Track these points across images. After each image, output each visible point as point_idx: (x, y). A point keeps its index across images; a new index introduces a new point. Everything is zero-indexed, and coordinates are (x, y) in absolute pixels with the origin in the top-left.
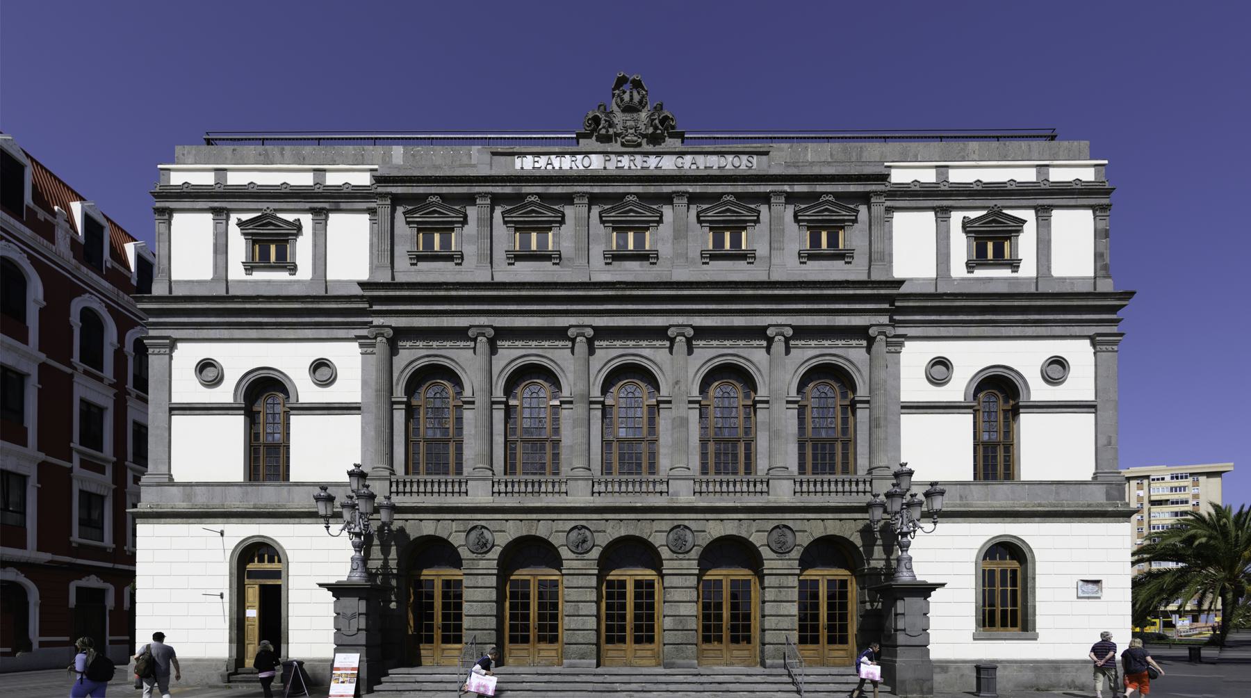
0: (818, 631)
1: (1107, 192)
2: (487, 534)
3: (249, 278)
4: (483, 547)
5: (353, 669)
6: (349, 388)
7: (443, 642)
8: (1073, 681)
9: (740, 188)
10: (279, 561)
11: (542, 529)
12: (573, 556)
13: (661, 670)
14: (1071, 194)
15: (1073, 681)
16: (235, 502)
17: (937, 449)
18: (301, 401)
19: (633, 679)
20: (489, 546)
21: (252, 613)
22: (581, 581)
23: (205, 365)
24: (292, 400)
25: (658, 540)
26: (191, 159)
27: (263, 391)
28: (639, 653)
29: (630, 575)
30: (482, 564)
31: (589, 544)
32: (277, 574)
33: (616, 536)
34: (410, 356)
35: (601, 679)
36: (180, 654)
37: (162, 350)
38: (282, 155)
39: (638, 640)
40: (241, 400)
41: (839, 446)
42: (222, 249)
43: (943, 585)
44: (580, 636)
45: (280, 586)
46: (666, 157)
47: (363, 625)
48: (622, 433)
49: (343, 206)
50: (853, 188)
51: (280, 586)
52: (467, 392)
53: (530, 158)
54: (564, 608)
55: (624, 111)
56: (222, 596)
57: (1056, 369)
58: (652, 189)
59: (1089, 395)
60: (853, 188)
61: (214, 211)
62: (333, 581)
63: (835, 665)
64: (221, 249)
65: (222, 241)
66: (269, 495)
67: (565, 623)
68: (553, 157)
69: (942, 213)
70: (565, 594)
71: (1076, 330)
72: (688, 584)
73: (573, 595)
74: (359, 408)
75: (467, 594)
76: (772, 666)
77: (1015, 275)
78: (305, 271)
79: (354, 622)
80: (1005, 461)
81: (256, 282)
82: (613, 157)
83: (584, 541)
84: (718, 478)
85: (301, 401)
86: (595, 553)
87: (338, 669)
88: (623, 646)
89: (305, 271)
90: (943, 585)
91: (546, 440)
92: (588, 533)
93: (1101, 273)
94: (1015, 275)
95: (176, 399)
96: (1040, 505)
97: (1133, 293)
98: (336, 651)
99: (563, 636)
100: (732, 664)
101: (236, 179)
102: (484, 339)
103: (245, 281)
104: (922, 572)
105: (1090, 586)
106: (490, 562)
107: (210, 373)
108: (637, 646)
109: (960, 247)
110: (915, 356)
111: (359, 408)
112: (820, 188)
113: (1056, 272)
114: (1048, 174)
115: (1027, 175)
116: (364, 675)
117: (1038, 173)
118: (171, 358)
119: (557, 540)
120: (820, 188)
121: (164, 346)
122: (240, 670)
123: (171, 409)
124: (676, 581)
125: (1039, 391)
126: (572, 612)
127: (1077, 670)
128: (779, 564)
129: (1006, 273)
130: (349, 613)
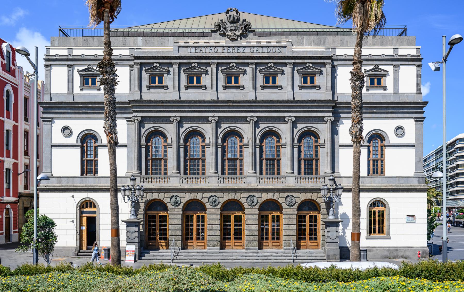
0: (306, 235)
1: (421, 60)
2: (178, 199)
3: (81, 92)
4: (177, 204)
5: (133, 251)
6: (410, 137)
8: (403, 255)
9: (275, 61)
10: (95, 207)
12: (211, 207)
13: (244, 251)
15: (403, 255)
16: (78, 184)
18: (103, 143)
19: (234, 254)
20: (179, 203)
21: (84, 228)
22: (213, 216)
23: (65, 129)
24: (99, 142)
25: (243, 200)
26: (81, 45)
27: (87, 136)
28: (236, 244)
30: (176, 210)
31: (217, 202)
32: (95, 212)
33: (227, 199)
35: (222, 254)
37: (48, 123)
38: (93, 40)
41: (314, 162)
42: (71, 80)
44: (213, 238)
45: (95, 218)
46: (246, 48)
47: (137, 235)
48: (230, 156)
49: (119, 63)
50: (319, 61)
51: (95, 218)
52: (169, 141)
53: (194, 48)
54: (207, 227)
55: (230, 23)
56: (73, 221)
58: (241, 61)
59: (413, 141)
60: (319, 61)
61: (68, 66)
62: (125, 220)
63: (312, 249)
64: (71, 81)
65: (71, 77)
66: (90, 181)
67: (207, 233)
68: (203, 48)
70: (207, 221)
72: (254, 218)
73: (211, 222)
74: (126, 146)
75: (170, 222)
78: (390, 89)
79: (134, 234)
80: (381, 166)
82: (226, 48)
83: (215, 201)
84: (266, 176)
85: (103, 143)
86: (219, 206)
87: (128, 251)
88: (230, 241)
89: (390, 89)
91: (199, 159)
92: (216, 198)
95: (53, 142)
96: (392, 186)
97: (427, 102)
98: (127, 244)
99: (207, 238)
100: (273, 248)
101: (77, 52)
102: (176, 121)
105: (411, 218)
106: (179, 210)
107: (67, 132)
108: (236, 241)
110: (59, 124)
111: (126, 146)
112: (306, 61)
113: (401, 91)
114: (398, 51)
115: (389, 52)
116: (137, 253)
118: (51, 126)
119: (205, 200)
120: (306, 61)
121: (49, 121)
122: (81, 251)
123: (52, 146)
124: (250, 217)
125: (392, 139)
126: (210, 228)
127: (405, 251)
128: (289, 210)
129: (382, 91)
130: (132, 231)
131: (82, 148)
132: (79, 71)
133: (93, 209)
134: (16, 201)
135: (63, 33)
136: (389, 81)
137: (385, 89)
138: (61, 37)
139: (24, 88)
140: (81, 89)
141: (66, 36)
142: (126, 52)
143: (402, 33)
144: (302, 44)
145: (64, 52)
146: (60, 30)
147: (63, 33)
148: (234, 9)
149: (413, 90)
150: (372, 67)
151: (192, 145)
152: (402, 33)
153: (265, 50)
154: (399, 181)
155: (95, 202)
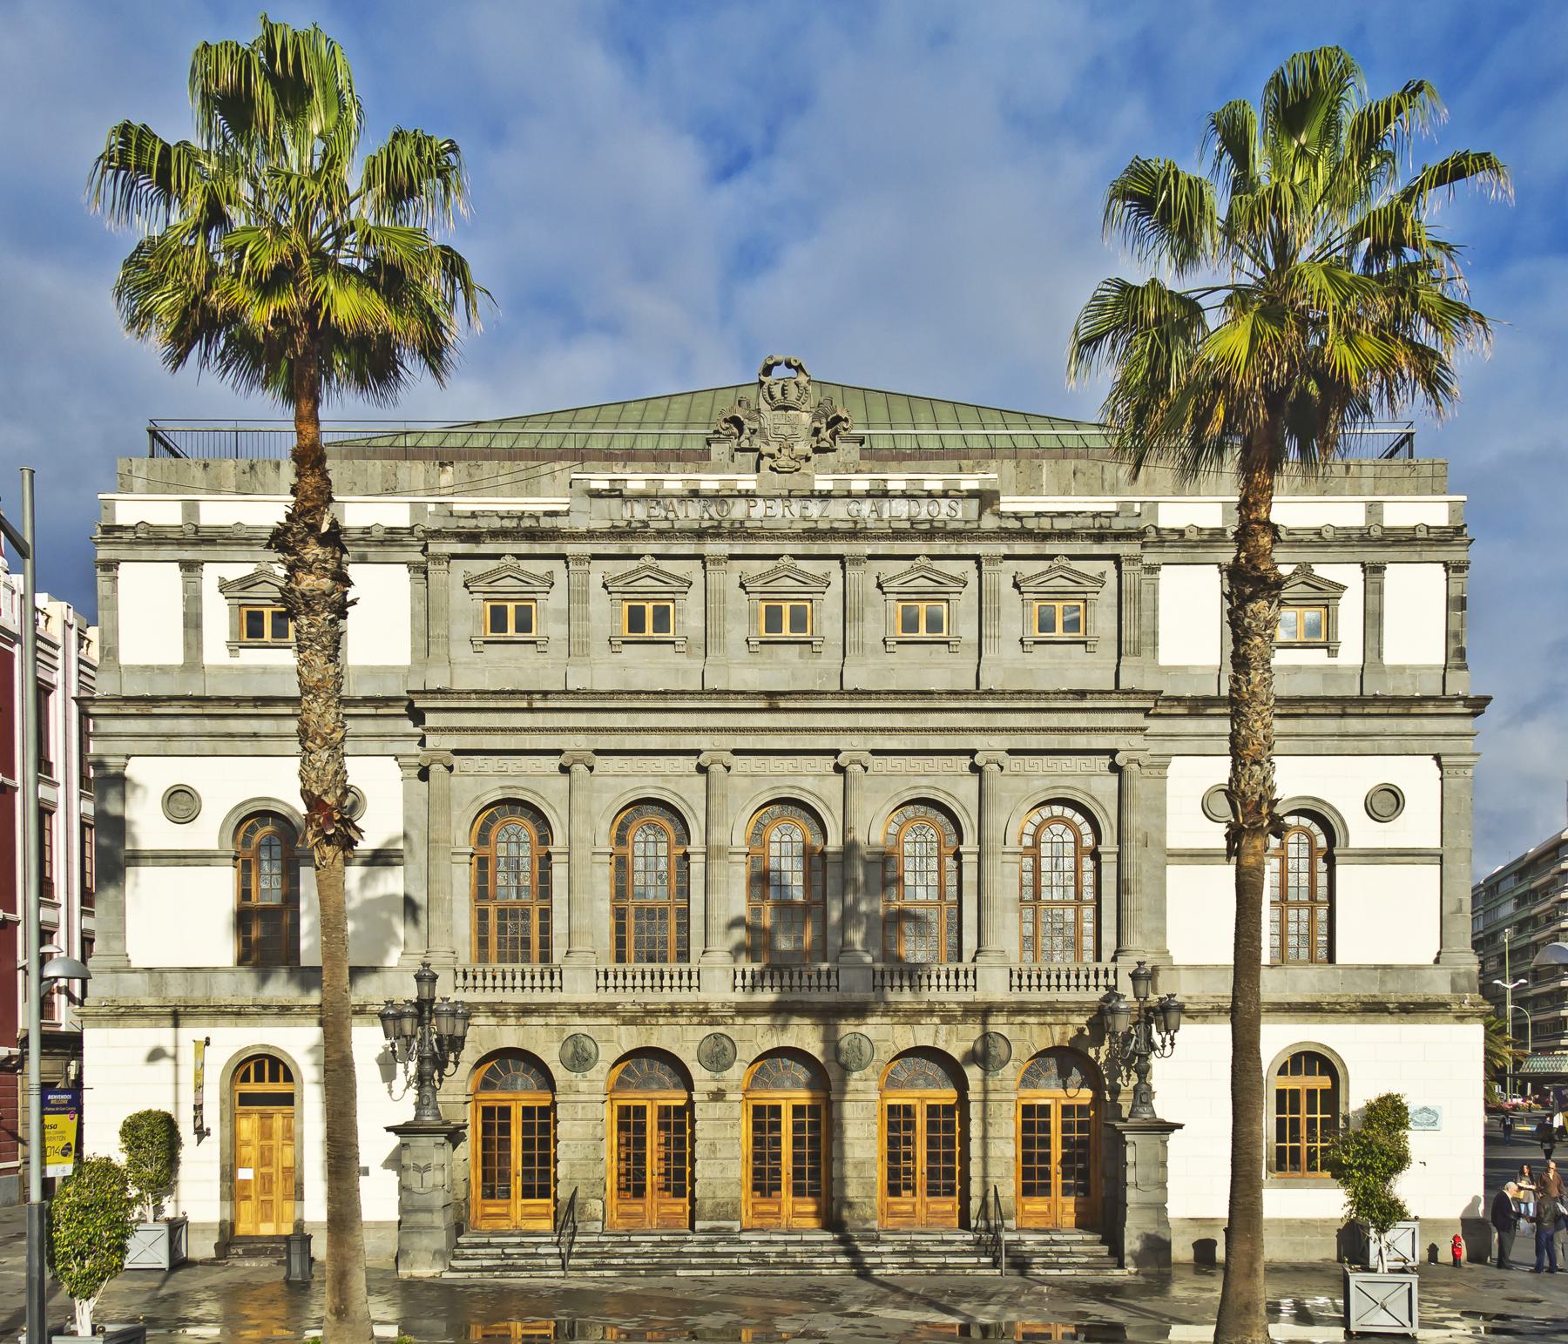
6: (1419, 824)
7: (525, 1196)
10: (289, 1077)
11: (663, 1037)
14: (1408, 541)
17: (1195, 922)
29: (520, 1097)
34: (483, 782)
36: (192, 1219)
39: (528, 1192)
40: (230, 848)
43: (1180, 1126)
57: (1386, 802)
64: (193, 623)
69: (189, 567)
71: (1415, 745)
76: (703, 1231)
77: (1332, 661)
81: (246, 670)
89: (1351, 653)
90: (1180, 1126)
93: (1454, 662)
94: (1332, 661)
97: (1488, 699)
103: (230, 668)
104: (1163, 1109)
109: (218, 617)
112: (1049, 548)
117: (185, 508)
120: (1049, 548)
125: (1362, 832)
131: (245, 868)
132: (224, 586)
133: (280, 1087)
134: (10, 1058)
135: (166, 446)
136: (1350, 611)
137: (1331, 648)
138: (156, 461)
139: (59, 654)
140: (235, 647)
141: (177, 456)
142: (393, 513)
143: (1397, 448)
144: (1032, 488)
145: (165, 512)
146: (153, 433)
147: (166, 446)
148: (778, 358)
149: (1435, 654)
150: (249, 569)
151: (637, 853)
152: (1397, 448)
153: (866, 507)
154: (1383, 982)
155: (288, 1063)
